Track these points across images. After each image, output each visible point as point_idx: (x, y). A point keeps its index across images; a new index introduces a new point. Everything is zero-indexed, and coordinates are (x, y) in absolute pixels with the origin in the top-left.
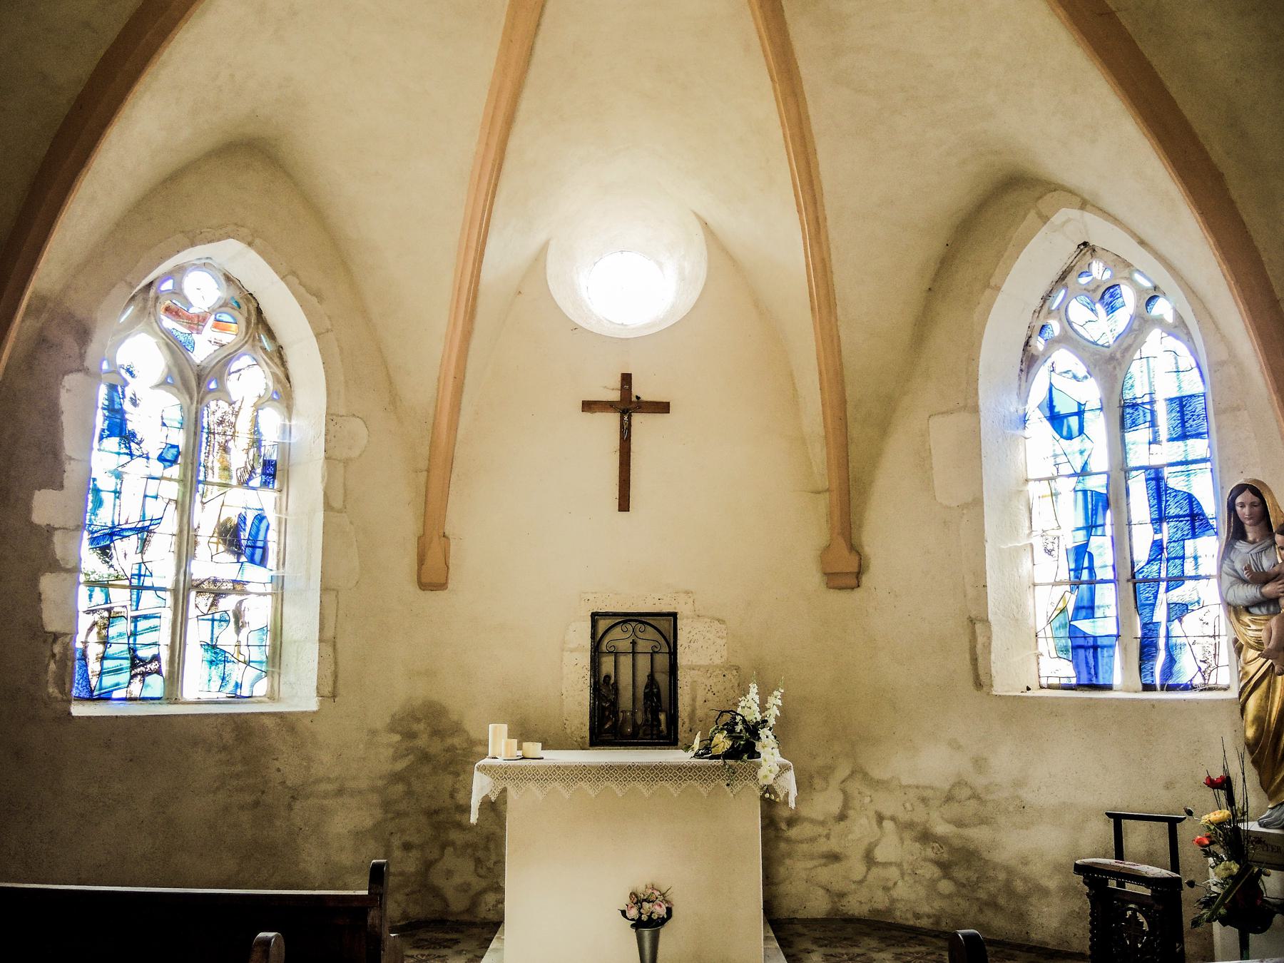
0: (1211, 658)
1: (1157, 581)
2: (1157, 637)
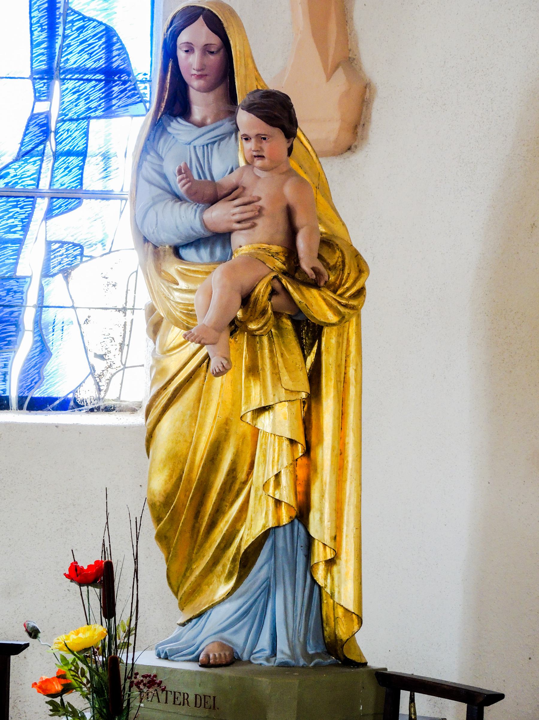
0: (114, 349)
1: (31, 197)
2: (22, 306)
